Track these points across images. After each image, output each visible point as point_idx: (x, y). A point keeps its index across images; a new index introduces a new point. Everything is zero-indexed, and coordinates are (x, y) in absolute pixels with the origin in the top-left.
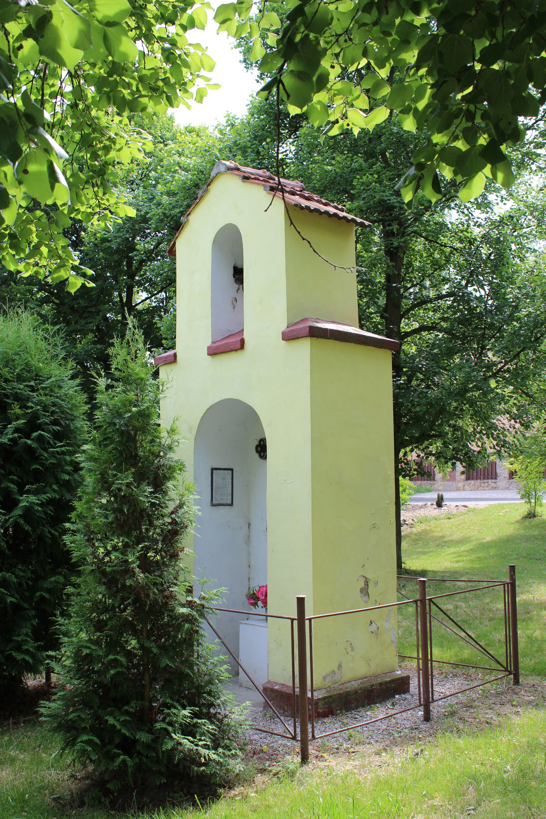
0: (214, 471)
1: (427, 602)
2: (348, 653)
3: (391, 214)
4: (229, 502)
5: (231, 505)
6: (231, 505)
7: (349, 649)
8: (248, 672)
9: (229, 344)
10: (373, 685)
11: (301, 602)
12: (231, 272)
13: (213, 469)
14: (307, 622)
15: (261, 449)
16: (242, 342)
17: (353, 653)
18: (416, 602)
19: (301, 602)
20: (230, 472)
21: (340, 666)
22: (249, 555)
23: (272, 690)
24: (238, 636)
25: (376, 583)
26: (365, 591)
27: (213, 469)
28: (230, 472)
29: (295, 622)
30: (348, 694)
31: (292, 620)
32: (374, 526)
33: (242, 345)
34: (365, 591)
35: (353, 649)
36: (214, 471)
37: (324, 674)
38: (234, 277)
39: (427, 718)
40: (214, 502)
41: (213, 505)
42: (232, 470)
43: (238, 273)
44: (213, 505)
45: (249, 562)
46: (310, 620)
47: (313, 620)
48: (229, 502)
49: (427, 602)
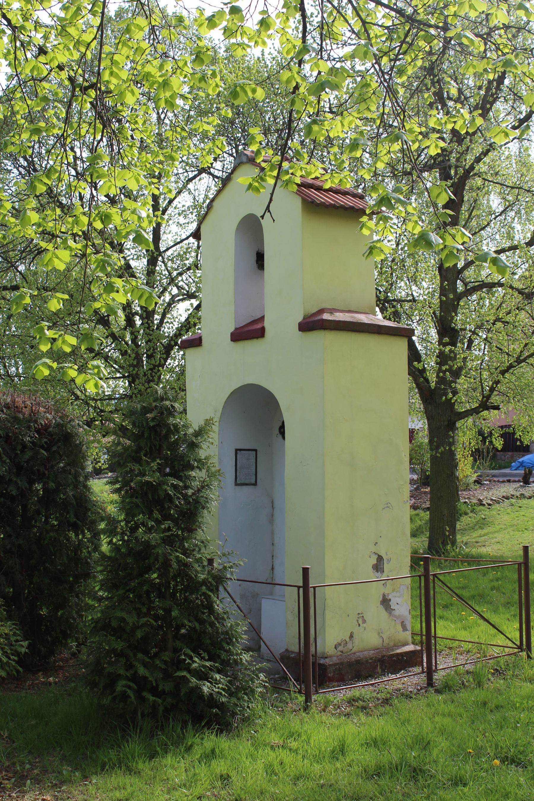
0: (238, 452)
1: (431, 577)
2: (359, 625)
3: (112, 521)
4: (253, 481)
5: (255, 484)
6: (255, 484)
7: (360, 621)
8: (268, 644)
9: (250, 331)
10: (384, 656)
11: (306, 571)
12: (254, 258)
13: (237, 450)
14: (311, 590)
15: (282, 430)
16: (263, 330)
17: (364, 625)
18: (420, 576)
19: (306, 571)
20: (254, 452)
21: (351, 636)
22: (273, 533)
23: (289, 658)
24: (260, 610)
25: (389, 561)
26: (378, 567)
27: (237, 450)
28: (254, 452)
29: (301, 590)
30: (358, 662)
31: (299, 587)
32: (388, 506)
33: (261, 333)
34: (378, 567)
35: (364, 621)
36: (238, 452)
37: (336, 643)
38: (257, 263)
39: (430, 683)
40: (238, 482)
41: (236, 484)
42: (256, 450)
43: (260, 258)
44: (236, 484)
45: (273, 539)
46: (314, 588)
47: (317, 588)
48: (253, 481)
49: (431, 577)
